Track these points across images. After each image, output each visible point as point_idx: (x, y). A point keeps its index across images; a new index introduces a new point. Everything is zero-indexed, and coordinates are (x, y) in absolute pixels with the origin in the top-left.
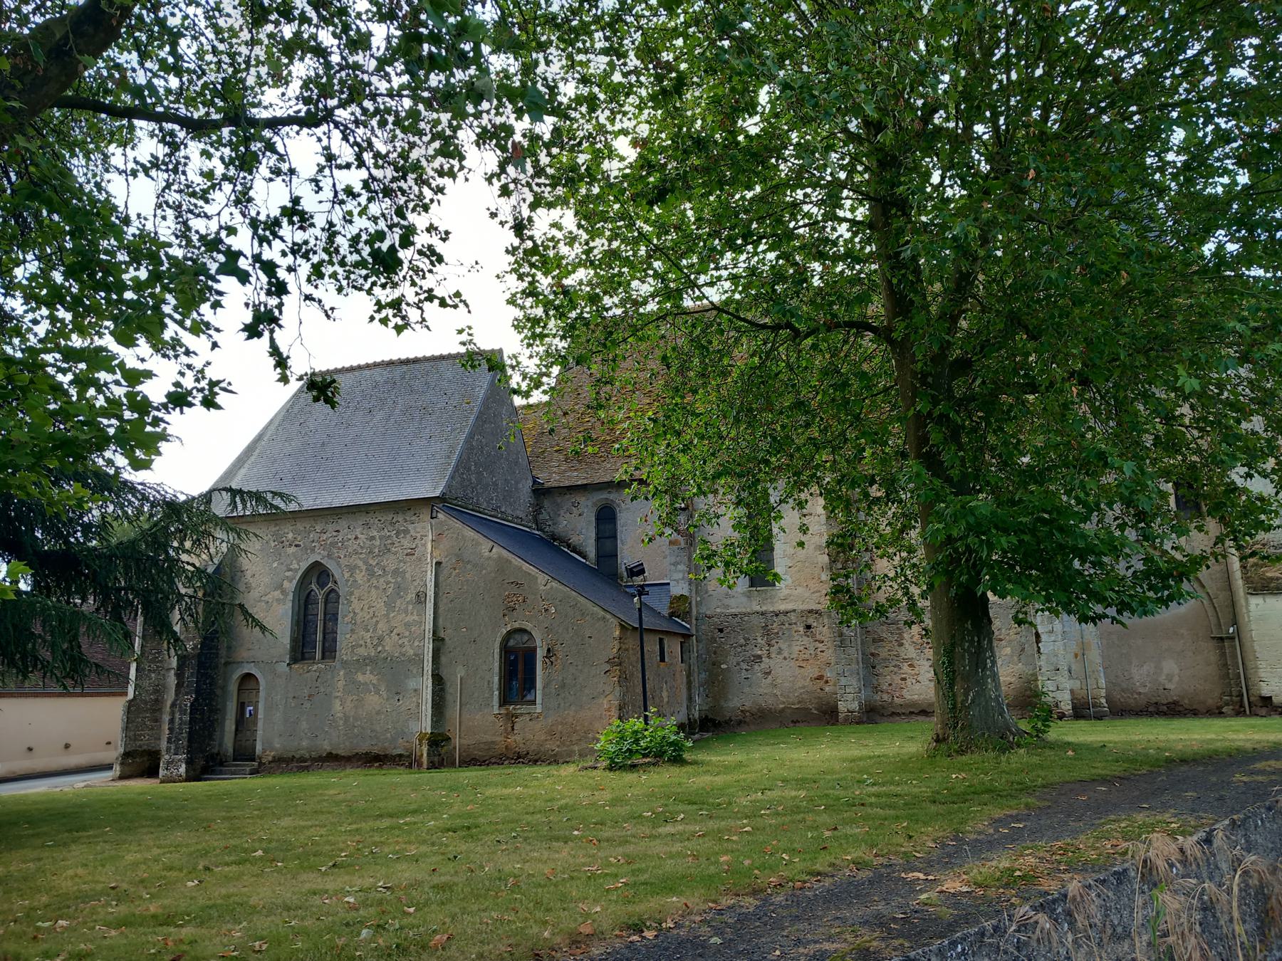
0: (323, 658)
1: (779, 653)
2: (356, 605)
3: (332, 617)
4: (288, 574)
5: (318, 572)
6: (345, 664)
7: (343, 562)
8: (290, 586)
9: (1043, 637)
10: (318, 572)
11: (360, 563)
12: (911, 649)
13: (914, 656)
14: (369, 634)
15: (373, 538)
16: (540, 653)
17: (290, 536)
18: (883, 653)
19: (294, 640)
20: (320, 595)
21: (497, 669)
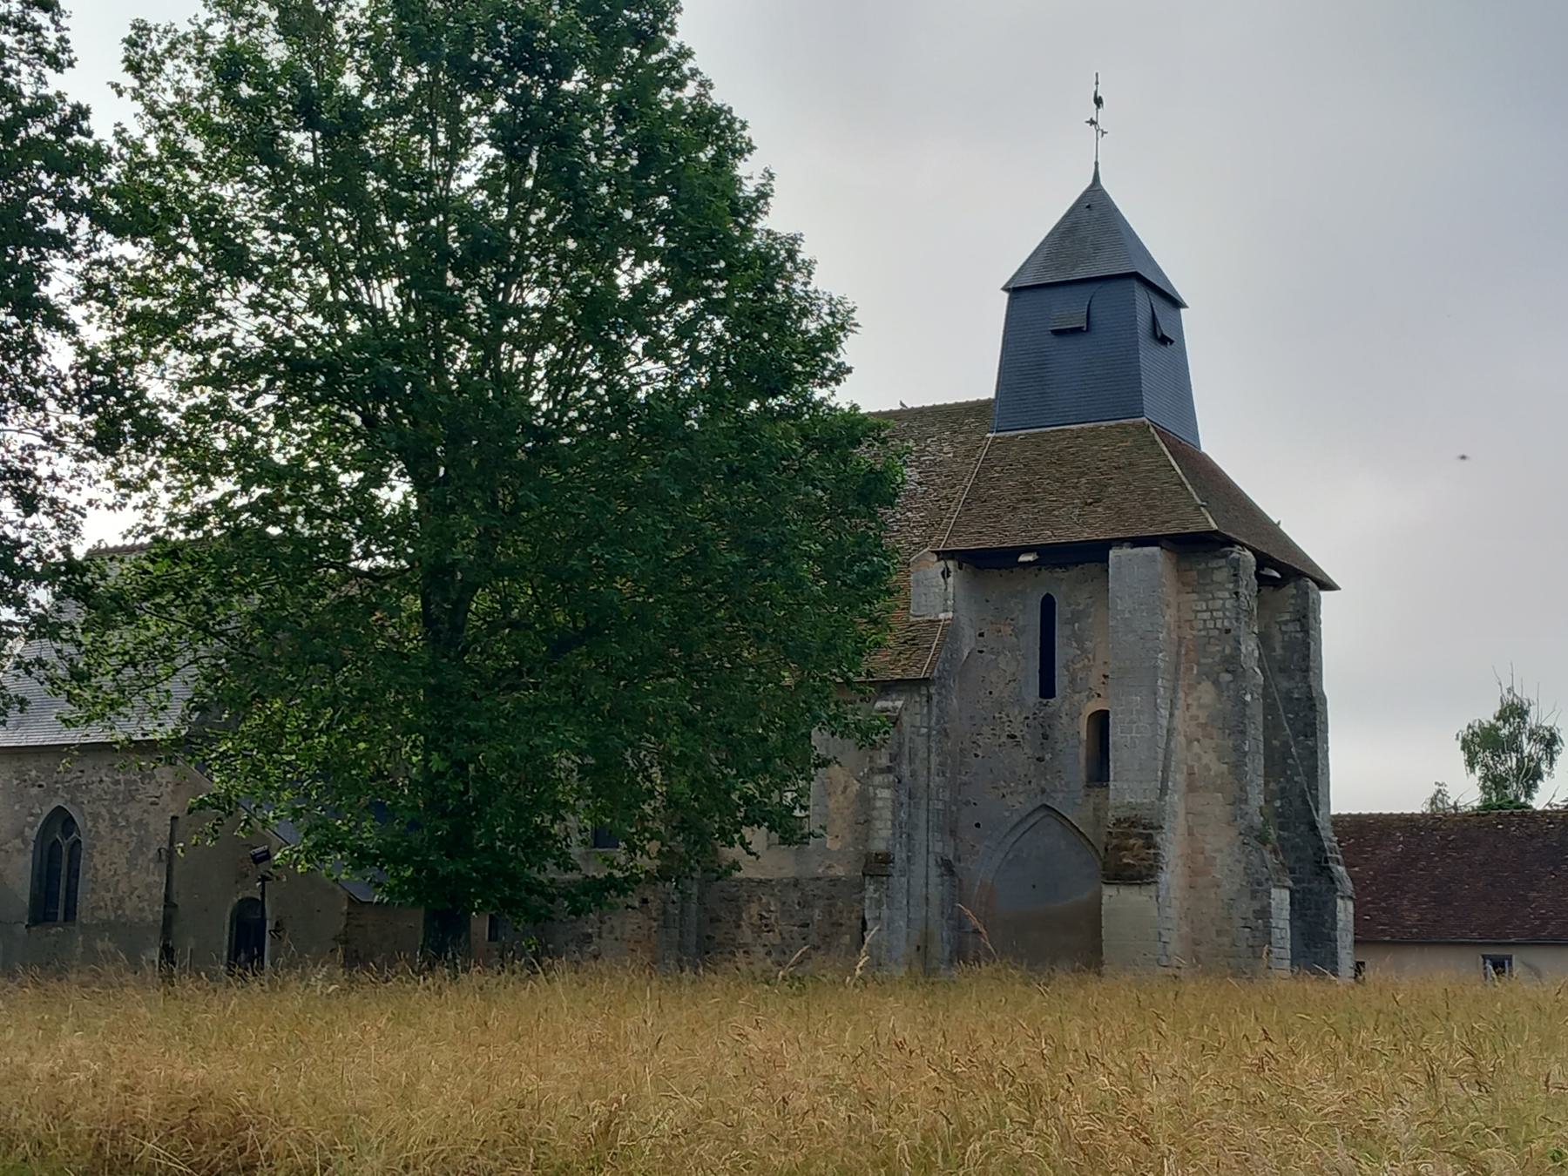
0: (66, 920)
1: (611, 932)
2: (97, 860)
3: (74, 874)
4: (31, 819)
5: (61, 820)
6: (83, 926)
7: (87, 808)
8: (31, 834)
9: (869, 924)
10: (61, 820)
11: (104, 812)
12: (748, 932)
13: (749, 940)
14: (110, 895)
15: (117, 782)
16: (269, 926)
17: (33, 773)
18: (719, 938)
19: (34, 898)
20: (65, 844)
21: (226, 943)
